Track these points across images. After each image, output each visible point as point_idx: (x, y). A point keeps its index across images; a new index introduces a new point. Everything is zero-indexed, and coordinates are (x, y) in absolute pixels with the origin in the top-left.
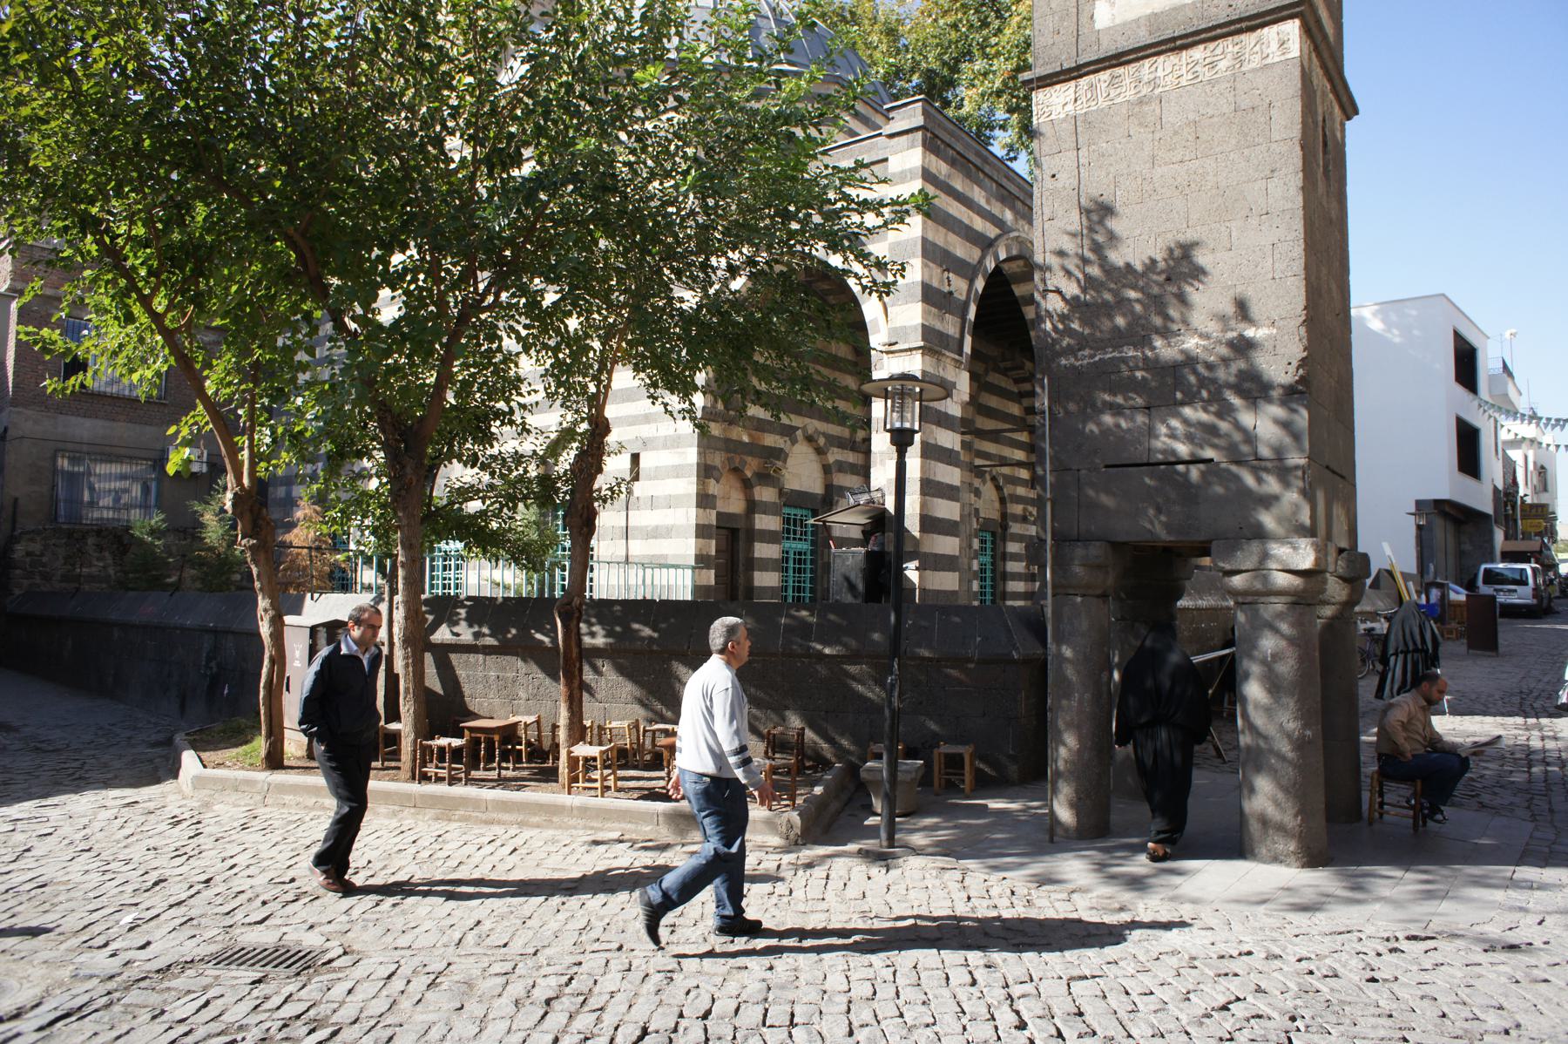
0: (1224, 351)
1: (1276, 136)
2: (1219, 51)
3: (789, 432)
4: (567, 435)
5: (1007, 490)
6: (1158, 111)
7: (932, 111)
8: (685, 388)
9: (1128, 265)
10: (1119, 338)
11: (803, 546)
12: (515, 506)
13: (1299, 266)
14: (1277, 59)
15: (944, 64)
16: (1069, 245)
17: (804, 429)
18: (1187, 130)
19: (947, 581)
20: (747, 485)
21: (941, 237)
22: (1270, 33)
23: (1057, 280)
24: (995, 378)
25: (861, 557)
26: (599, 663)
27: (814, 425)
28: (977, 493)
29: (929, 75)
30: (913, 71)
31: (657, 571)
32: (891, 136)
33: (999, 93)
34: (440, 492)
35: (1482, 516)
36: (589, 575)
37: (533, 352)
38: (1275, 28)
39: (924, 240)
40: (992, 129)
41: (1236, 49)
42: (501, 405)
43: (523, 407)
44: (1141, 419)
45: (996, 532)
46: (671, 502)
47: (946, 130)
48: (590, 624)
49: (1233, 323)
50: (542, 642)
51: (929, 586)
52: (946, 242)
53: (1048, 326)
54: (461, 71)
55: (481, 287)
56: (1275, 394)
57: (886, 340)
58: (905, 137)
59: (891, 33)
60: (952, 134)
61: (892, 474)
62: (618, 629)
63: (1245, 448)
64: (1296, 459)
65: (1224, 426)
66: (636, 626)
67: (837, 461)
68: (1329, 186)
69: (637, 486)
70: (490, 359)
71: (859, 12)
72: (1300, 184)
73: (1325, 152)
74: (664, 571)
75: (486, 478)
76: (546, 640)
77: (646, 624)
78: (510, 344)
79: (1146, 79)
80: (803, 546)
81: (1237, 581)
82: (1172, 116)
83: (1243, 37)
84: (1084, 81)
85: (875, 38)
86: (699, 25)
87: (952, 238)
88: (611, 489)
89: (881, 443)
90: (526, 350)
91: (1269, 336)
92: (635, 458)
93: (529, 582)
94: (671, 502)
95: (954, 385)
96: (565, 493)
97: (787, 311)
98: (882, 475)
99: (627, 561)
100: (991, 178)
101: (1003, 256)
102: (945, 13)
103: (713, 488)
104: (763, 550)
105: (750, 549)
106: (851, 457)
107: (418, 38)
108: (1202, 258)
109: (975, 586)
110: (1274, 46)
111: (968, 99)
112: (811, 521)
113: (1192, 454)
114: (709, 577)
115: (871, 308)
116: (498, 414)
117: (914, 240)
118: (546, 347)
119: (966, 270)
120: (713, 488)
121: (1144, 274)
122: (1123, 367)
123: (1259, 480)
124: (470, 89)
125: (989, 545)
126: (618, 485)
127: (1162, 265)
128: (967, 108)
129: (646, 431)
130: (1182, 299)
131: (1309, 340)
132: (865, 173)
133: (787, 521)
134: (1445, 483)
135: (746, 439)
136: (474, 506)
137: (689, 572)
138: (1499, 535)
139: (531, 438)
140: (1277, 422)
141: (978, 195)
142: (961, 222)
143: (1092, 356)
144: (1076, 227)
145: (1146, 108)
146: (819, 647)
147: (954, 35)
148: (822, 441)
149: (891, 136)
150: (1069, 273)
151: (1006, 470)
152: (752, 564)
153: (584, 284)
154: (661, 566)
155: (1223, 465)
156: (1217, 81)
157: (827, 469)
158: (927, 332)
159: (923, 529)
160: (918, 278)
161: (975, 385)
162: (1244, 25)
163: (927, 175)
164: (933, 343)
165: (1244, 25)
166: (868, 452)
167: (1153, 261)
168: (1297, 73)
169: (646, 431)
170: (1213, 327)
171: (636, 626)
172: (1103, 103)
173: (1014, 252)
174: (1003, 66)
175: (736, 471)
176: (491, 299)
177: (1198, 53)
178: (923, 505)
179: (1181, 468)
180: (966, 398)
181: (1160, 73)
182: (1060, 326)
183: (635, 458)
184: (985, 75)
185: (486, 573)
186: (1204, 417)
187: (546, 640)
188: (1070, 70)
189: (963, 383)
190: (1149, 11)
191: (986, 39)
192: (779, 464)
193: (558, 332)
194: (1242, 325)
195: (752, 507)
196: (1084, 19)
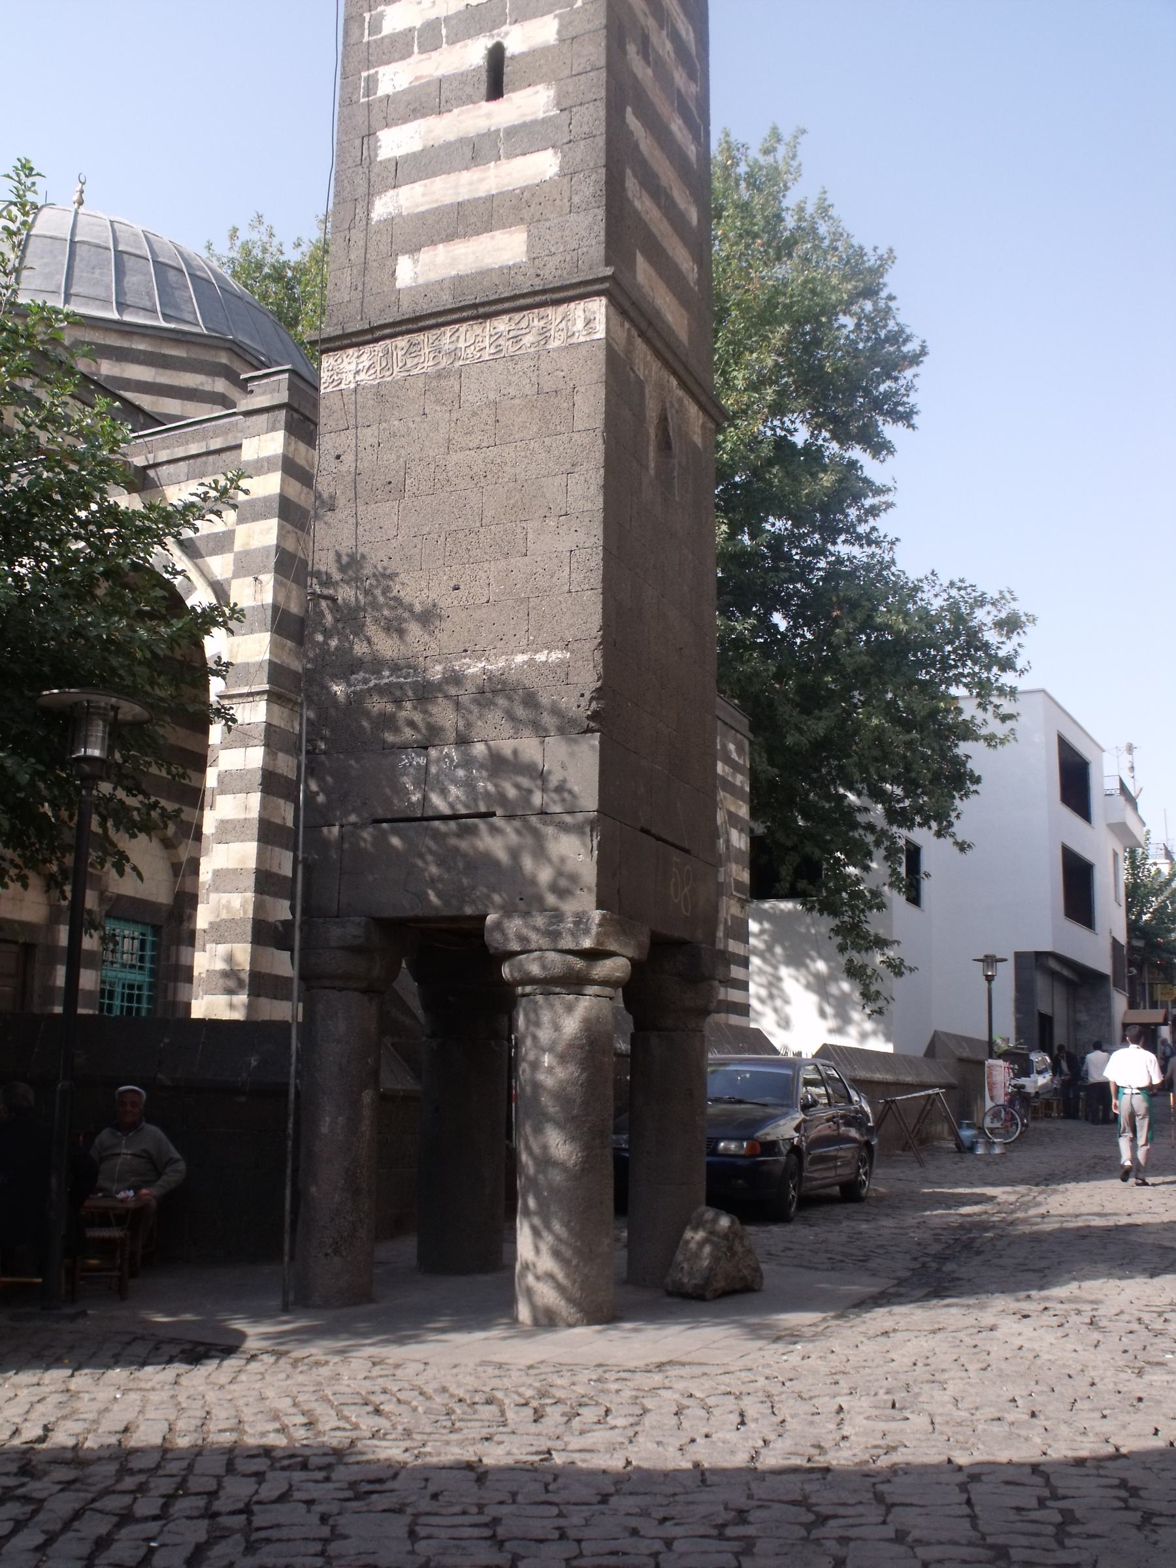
1: (579, 425)
2: (524, 324)
13: (596, 578)
14: (582, 339)
22: (578, 310)
35: (1102, 977)
38: (581, 305)
41: (542, 323)
58: (265, 416)
72: (601, 482)
82: (471, 397)
91: (562, 661)
110: (580, 324)
117: (266, 549)
131: (605, 667)
134: (1045, 928)
138: (1120, 1002)
145: (443, 383)
172: (398, 374)
177: (502, 324)
181: (461, 344)
190: (454, 273)
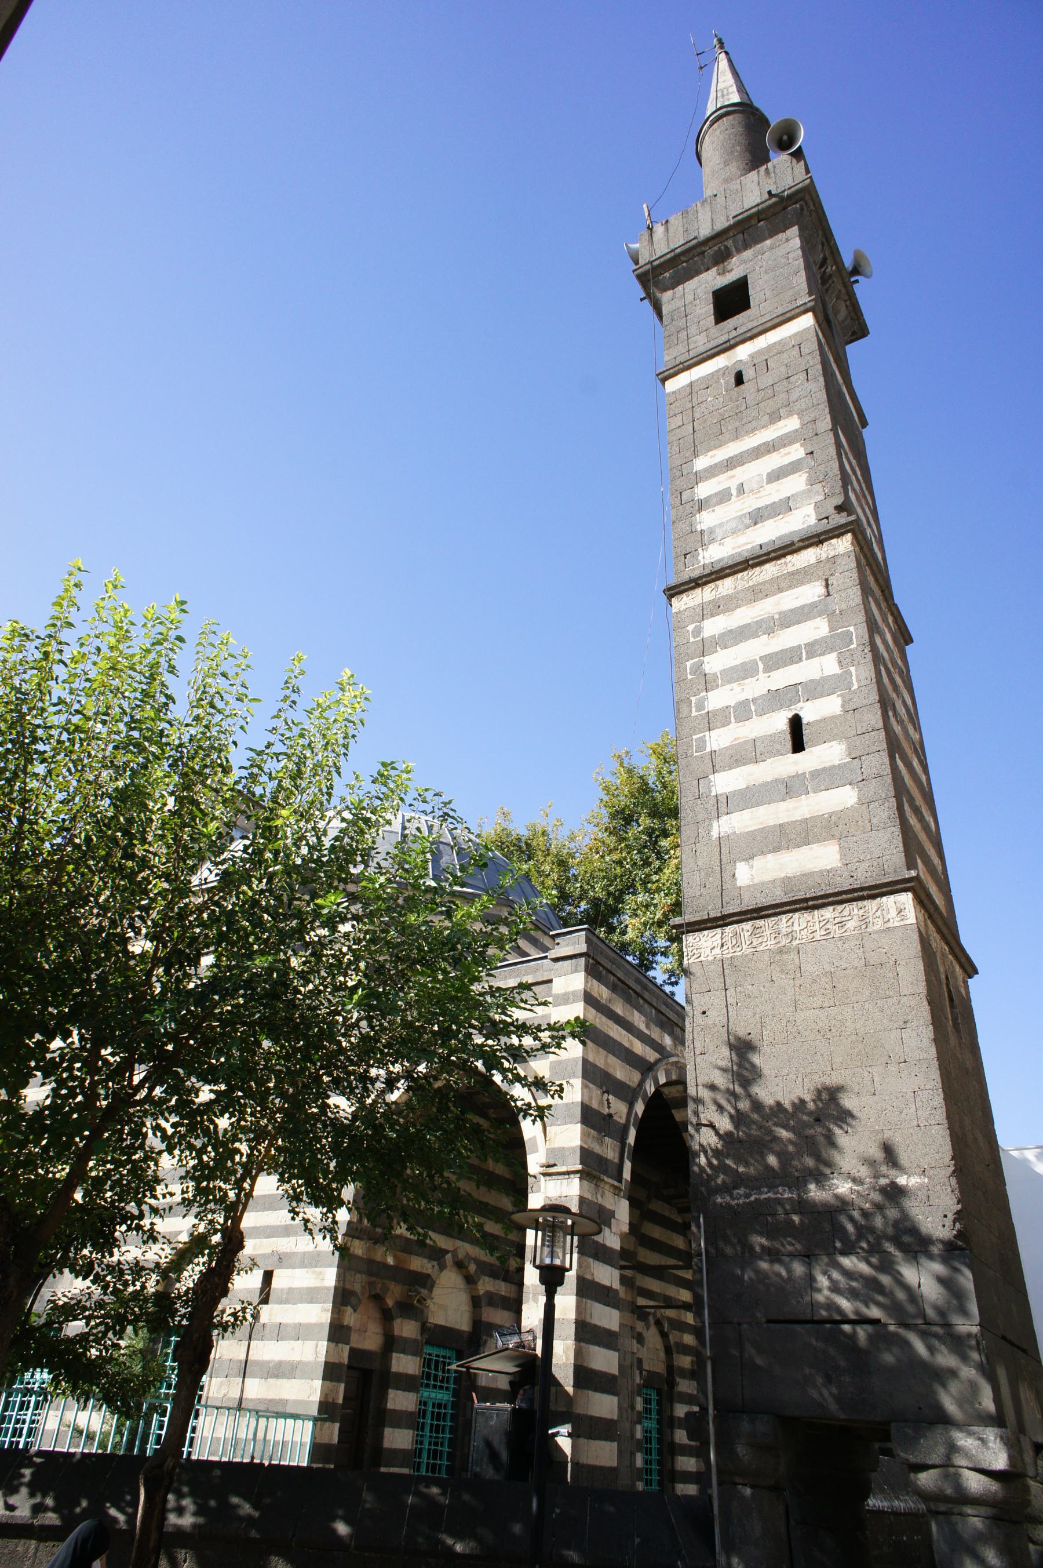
0: (877, 1197)
3: (437, 1255)
4: (198, 1243)
5: (672, 1338)
6: (797, 961)
7: (595, 940)
8: (330, 1201)
9: (778, 1104)
10: (770, 1178)
11: (444, 1396)
12: (123, 1330)
13: (941, 1114)
14: (897, 924)
15: (609, 894)
16: (721, 1081)
17: (454, 1253)
18: (824, 979)
19: (604, 1454)
20: (387, 1317)
21: (601, 1059)
22: (889, 901)
23: (709, 1114)
24: (657, 1206)
25: (506, 1416)
26: (181, 1554)
27: (465, 1248)
28: (640, 1339)
29: (595, 902)
30: (581, 898)
31: (272, 1421)
32: (556, 960)
33: (660, 924)
34: (40, 1307)
36: (192, 1423)
37: (177, 1152)
39: (585, 1061)
40: (654, 954)
42: (132, 1207)
43: (155, 1211)
44: (799, 1268)
45: (661, 1388)
46: (300, 1332)
47: (607, 957)
48: (180, 1496)
49: (884, 1169)
50: (115, 1520)
51: (585, 1460)
52: (606, 1064)
53: (703, 1160)
54: (160, 877)
55: (136, 1080)
56: (935, 1250)
57: (544, 1161)
58: (569, 962)
59: (562, 864)
60: (613, 962)
61: (540, 1314)
62: (213, 1503)
63: (911, 1309)
64: (968, 1326)
65: (885, 1279)
66: (235, 1500)
67: (488, 1293)
68: (960, 1038)
69: (264, 1309)
70: (130, 1155)
71: (534, 844)
72: (932, 1036)
73: (952, 1006)
74: (281, 1421)
75: (97, 1291)
76: (121, 1518)
77: (246, 1499)
78: (154, 1141)
79: (784, 931)
80: (444, 1396)
81: (926, 1479)
83: (865, 903)
84: (728, 930)
85: (547, 868)
86: (383, 855)
87: (613, 1060)
88: (234, 1315)
89: (531, 1276)
90: (170, 1150)
92: (268, 1276)
93: (119, 1431)
94: (300, 1332)
95: (612, 1214)
96: (183, 1316)
97: (440, 1128)
98: (532, 1315)
99: (240, 1407)
100: (650, 1004)
101: (662, 1080)
102: (611, 851)
103: (350, 1318)
104: (400, 1400)
105: (383, 1397)
106: (503, 1288)
107: (125, 849)
108: (848, 1102)
109: (639, 1460)
110: (893, 913)
111: (632, 926)
112: (454, 1367)
113: (857, 1312)
114: (333, 1432)
115: (529, 1129)
116: (126, 1217)
117: (575, 1060)
118: (191, 1147)
119: (627, 1094)
120: (350, 1318)
121: (793, 1115)
122: (780, 1210)
123: (931, 1349)
124: (162, 894)
125: (654, 1406)
126: (244, 1310)
127: (811, 1106)
128: (631, 935)
129: (284, 1245)
130: (832, 1143)
131: (961, 1192)
132: (526, 995)
133: (427, 1363)
135: (390, 1261)
136: (75, 1327)
137: (310, 1424)
139: (156, 1248)
140: (941, 1280)
141: (638, 1020)
142: (621, 1044)
143: (748, 1196)
144: (725, 1063)
145: (785, 957)
146: (450, 1541)
147: (619, 871)
148: (472, 1268)
149: (556, 960)
150: (720, 1108)
151: (670, 1313)
152: (385, 1418)
153: (241, 1081)
154: (278, 1415)
155: (892, 1328)
156: (847, 938)
157: (476, 1302)
158: (586, 1155)
159: (577, 1385)
160: (578, 1098)
161: (637, 1212)
162: (865, 893)
163: (589, 999)
164: (592, 1167)
165: (865, 893)
166: (520, 1284)
167: (802, 1102)
168: (916, 937)
169: (284, 1245)
170: (863, 1172)
171: (235, 1500)
173: (674, 1077)
174: (663, 901)
175: (377, 1298)
176: (144, 1093)
177: (828, 913)
178: (578, 1353)
179: (847, 1328)
180: (626, 1229)
181: (796, 927)
182: (715, 1162)
183: (268, 1276)
184: (647, 906)
185: (70, 1416)
186: (864, 1268)
187: (121, 1518)
188: (716, 919)
189: (622, 1211)
190: (783, 875)
191: (648, 876)
192: (424, 1292)
193: (206, 1132)
194: (893, 1172)
195: (391, 1343)
196: (727, 877)
